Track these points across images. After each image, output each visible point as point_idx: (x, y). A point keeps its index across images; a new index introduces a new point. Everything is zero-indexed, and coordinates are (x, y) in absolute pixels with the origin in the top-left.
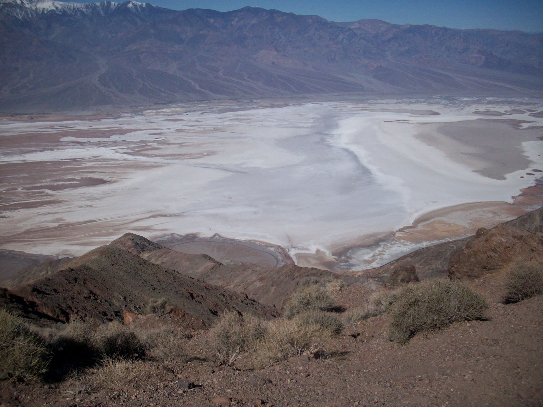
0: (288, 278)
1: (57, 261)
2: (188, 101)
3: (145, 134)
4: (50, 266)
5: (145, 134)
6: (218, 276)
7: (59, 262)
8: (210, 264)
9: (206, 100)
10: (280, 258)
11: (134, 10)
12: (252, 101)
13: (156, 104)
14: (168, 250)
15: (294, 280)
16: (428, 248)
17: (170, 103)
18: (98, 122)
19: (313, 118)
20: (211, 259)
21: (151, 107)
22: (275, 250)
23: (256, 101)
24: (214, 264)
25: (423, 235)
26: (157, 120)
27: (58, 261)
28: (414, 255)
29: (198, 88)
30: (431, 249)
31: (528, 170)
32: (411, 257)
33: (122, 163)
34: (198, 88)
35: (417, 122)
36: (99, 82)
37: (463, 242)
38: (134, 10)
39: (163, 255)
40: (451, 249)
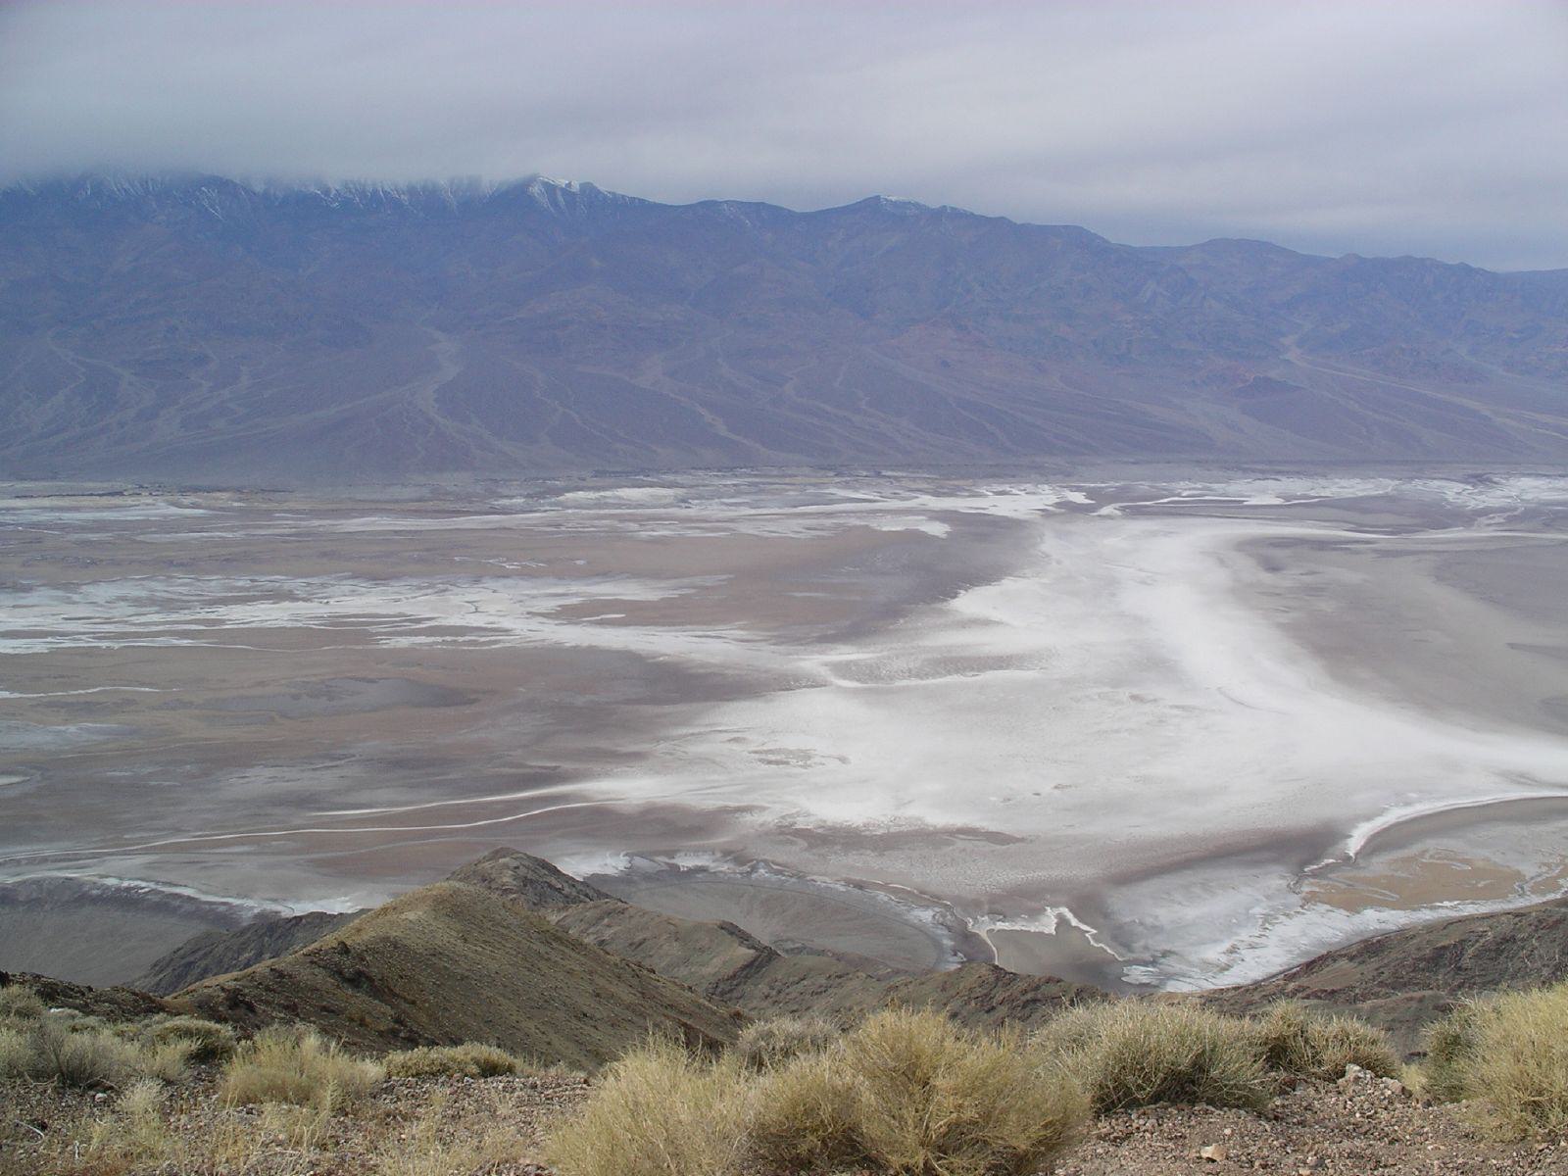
0: (973, 1003)
1: (290, 920)
2: (693, 468)
3: (773, 652)
4: (271, 937)
5: (773, 652)
6: (763, 988)
7: (297, 924)
8: (744, 953)
9: (746, 467)
10: (948, 943)
11: (544, 201)
12: (878, 475)
13: (599, 474)
14: (620, 904)
15: (992, 1013)
16: (1404, 935)
17: (643, 471)
18: (711, 627)
19: (340, 1051)
20: (744, 938)
21: (584, 484)
22: (934, 917)
23: (889, 473)
24: (752, 951)
25: (1387, 892)
26: (811, 657)
27: (294, 922)
28: (1360, 953)
29: (722, 430)
30: (1413, 937)
32: (1352, 959)
33: (495, 642)
34: (722, 430)
35: (827, 688)
36: (437, 406)
37: (1517, 919)
38: (544, 201)
39: (603, 919)
40: (1477, 941)
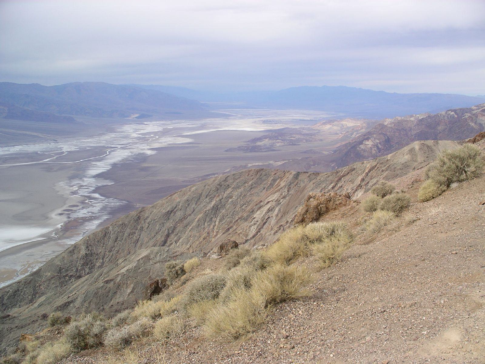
31: (65, 208)
37: (18, 284)
